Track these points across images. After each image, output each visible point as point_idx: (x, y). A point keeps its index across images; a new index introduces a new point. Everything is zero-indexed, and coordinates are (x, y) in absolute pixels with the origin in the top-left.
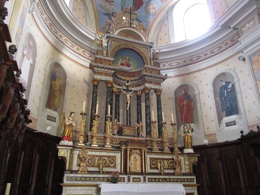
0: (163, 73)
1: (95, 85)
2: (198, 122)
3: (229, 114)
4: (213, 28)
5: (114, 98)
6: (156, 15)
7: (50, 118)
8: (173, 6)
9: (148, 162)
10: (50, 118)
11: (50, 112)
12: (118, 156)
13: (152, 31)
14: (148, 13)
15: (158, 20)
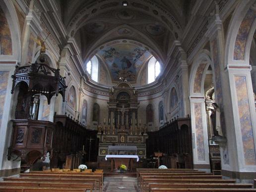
0: (139, 99)
1: (110, 110)
2: (153, 122)
3: (150, 122)
4: (160, 73)
5: (117, 113)
6: (140, 67)
7: (94, 124)
8: (148, 61)
9: (128, 139)
10: (94, 124)
11: (95, 122)
12: (117, 137)
13: (139, 76)
14: (135, 68)
15: (141, 70)
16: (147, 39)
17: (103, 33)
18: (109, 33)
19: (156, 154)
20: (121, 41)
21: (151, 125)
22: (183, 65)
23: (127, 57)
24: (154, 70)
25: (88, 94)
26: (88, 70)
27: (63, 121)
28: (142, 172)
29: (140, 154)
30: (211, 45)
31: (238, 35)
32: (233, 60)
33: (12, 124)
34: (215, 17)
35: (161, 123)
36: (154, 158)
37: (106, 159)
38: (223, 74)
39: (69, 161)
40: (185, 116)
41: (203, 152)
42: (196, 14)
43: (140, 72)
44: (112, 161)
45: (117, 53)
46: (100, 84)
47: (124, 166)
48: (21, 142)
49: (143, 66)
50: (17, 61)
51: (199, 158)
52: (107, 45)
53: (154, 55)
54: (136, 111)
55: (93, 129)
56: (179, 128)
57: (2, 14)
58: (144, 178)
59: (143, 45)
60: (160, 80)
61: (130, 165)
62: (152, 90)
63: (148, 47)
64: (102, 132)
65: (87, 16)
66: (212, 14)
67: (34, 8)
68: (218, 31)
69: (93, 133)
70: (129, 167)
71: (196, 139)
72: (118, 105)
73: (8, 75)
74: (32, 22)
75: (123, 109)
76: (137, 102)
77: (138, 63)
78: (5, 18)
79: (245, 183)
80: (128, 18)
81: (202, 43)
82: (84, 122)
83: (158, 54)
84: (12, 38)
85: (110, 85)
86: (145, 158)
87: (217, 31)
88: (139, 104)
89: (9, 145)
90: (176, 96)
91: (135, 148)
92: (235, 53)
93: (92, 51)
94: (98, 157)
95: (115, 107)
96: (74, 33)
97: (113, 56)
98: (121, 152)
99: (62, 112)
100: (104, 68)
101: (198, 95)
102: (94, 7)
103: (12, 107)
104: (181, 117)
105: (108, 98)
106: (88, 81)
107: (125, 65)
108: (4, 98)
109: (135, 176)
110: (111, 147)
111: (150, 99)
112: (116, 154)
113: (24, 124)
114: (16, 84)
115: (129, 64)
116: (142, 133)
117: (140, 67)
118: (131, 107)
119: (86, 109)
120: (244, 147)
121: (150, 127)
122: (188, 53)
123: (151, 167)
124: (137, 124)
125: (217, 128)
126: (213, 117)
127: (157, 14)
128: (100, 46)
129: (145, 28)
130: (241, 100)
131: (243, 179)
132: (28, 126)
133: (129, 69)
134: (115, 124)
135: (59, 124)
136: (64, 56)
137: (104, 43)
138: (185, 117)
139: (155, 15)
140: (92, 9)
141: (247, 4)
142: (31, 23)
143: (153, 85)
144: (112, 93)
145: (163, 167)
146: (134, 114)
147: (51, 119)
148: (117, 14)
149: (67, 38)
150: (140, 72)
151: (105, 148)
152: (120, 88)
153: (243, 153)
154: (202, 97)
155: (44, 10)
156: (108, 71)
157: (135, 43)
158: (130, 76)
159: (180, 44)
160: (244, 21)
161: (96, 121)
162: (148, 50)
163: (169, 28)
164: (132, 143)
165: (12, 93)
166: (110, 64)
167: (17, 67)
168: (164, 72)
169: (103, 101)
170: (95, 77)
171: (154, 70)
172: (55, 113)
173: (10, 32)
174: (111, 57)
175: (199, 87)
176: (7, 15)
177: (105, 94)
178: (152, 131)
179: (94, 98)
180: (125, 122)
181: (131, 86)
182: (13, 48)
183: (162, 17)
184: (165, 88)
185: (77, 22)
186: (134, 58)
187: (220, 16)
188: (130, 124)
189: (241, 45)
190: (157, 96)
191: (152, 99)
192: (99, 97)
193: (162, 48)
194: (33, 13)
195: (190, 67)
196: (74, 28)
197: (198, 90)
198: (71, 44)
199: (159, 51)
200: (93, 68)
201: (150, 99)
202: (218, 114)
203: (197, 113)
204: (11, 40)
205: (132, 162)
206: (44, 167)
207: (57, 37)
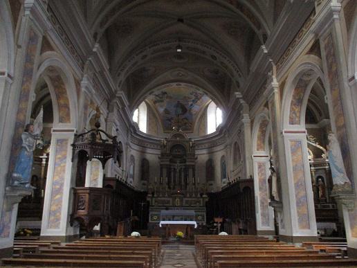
0: (197, 152)
1: (162, 167)
6: (197, 114)
7: (144, 184)
8: (207, 106)
10: (144, 184)
11: (143, 182)
12: (171, 199)
13: (196, 124)
14: (191, 114)
19: (216, 220)
20: (175, 84)
21: (212, 185)
22: (246, 119)
23: (181, 102)
24: (215, 118)
25: (136, 147)
26: (135, 119)
27: (113, 184)
28: (201, 238)
29: (199, 220)
30: (270, 105)
31: (292, 101)
32: (289, 125)
33: (72, 191)
34: (272, 80)
35: (224, 183)
36: (215, 225)
37: (161, 226)
38: (280, 139)
39: (120, 228)
40: (248, 177)
41: (267, 217)
43: (198, 119)
44: (167, 229)
45: (171, 98)
46: (150, 136)
47: (180, 233)
48: (82, 209)
49: (201, 113)
50: (6, 70)
51: (263, 223)
53: (213, 100)
54: (193, 167)
55: (142, 191)
56: (241, 191)
58: (213, 253)
60: (221, 130)
61: (187, 232)
62: (212, 141)
63: (208, 92)
64: (153, 194)
65: (136, 63)
66: (269, 74)
68: (336, 21)
69: (141, 196)
70: (187, 234)
71: (259, 203)
72: (171, 161)
73: (67, 143)
75: (178, 165)
76: (194, 157)
77: (196, 108)
79: (298, 245)
80: (182, 61)
82: (131, 182)
83: (219, 100)
84: (71, 108)
85: (162, 137)
86: (204, 224)
87: (334, 20)
88: (197, 158)
89: (71, 213)
90: (238, 151)
91: (192, 212)
92: (290, 118)
93: (140, 97)
94: (148, 224)
95: (168, 163)
97: (165, 102)
98: (175, 218)
99: (112, 173)
100: (154, 115)
101: (262, 153)
102: (144, 54)
103: (72, 173)
104: (243, 178)
105: (159, 152)
106: (135, 133)
107: (180, 111)
108: (64, 166)
109: (192, 243)
110: (164, 212)
111: (211, 153)
112: (169, 220)
113: (85, 191)
114: (76, 152)
115: (185, 110)
116: (201, 195)
117: (197, 114)
118: (187, 163)
119: (134, 167)
120: (298, 212)
121: (211, 187)
122: (251, 104)
123: (211, 233)
124: (194, 184)
125: (273, 193)
126: (270, 181)
128: (150, 91)
130: (296, 165)
131: (296, 242)
132: (89, 194)
133: (183, 117)
134: (169, 183)
135: (109, 186)
136: (113, 111)
137: (153, 88)
138: (248, 178)
140: (141, 55)
141: (298, 75)
142: (31, 11)
143: (213, 136)
144: (165, 146)
145: (224, 233)
146: (191, 171)
147: (100, 185)
149: (116, 91)
150: (198, 119)
151: (156, 213)
152: (173, 139)
153: (297, 218)
154: (300, 130)
156: (158, 118)
158: (186, 123)
159: (241, 96)
161: (146, 180)
162: (207, 94)
164: (189, 207)
165: (72, 161)
166: (161, 110)
167: (75, 135)
168: (228, 118)
169: (152, 155)
170: (143, 128)
171: (215, 118)
172: (104, 175)
173: (68, 102)
174: (162, 101)
175: (262, 145)
177: (156, 147)
178: (212, 191)
179: (143, 152)
180: (180, 182)
181: (188, 137)
182: (71, 117)
183: (222, 63)
184: (228, 141)
186: (190, 103)
188: (186, 184)
189: (297, 110)
190: (219, 149)
191: (213, 152)
192: (149, 151)
193: (223, 90)
194: (87, 77)
195: (252, 122)
196: (122, 78)
197: (261, 148)
198: (120, 98)
199: (219, 97)
200: (141, 115)
201: (211, 153)
202: (274, 179)
203: (260, 174)
204: (69, 109)
205: (189, 229)
206: (95, 235)
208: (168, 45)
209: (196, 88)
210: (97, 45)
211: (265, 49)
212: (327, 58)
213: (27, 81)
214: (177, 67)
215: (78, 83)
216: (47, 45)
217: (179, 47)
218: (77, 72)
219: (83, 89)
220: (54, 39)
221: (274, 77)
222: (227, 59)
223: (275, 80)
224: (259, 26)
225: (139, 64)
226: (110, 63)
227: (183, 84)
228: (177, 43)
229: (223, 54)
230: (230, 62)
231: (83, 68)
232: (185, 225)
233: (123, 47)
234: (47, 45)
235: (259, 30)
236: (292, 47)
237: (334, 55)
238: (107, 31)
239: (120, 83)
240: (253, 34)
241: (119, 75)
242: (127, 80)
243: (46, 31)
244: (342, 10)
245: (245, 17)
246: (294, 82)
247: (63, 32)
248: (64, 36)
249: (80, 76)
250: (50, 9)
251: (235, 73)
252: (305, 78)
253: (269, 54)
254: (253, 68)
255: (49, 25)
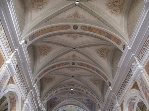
16: (83, 105)
17: (59, 102)
18: (63, 102)
42: (107, 99)
52: (61, 109)
57: (15, 102)
59: (81, 109)
65: (52, 95)
67: (13, 57)
68: (119, 110)
74: (27, 104)
78: (16, 104)
80: (73, 95)
81: (130, 83)
96: (45, 104)
127: (88, 94)
129: (82, 100)
137: (59, 108)
139: (87, 95)
142: (8, 65)
148: (68, 93)
155: (33, 96)
157: (77, 107)
160: (129, 106)
163: (94, 101)
176: (17, 103)
183: (91, 96)
185: (46, 99)
187: (118, 101)
196: (45, 102)
207: (36, 108)
208: (67, 87)
209: (80, 108)
210: (35, 84)
211: (111, 88)
212: (143, 90)
213: (13, 106)
214: (71, 98)
215: (23, 101)
216: (11, 81)
217: (73, 88)
218: (24, 96)
219: (25, 105)
220: (16, 79)
221: (117, 101)
222: (93, 94)
223: (117, 103)
224: (107, 79)
225: (53, 95)
226: (41, 93)
227: (73, 106)
228: (71, 87)
229: (91, 92)
230: (95, 95)
231: (27, 94)
232: (141, 28)
233: (48, 87)
234: (11, 81)
235: (107, 80)
236: (123, 87)
237: (146, 88)
238: (41, 80)
239: (44, 104)
240: (104, 82)
241: (43, 100)
242: (48, 102)
243: (13, 74)
244: (144, 69)
245: (100, 76)
246: (127, 103)
247: (21, 76)
248: (21, 79)
249: (25, 98)
250: (17, 66)
251: (97, 100)
252: (133, 101)
253: (113, 91)
254: (106, 97)
255: (15, 72)
